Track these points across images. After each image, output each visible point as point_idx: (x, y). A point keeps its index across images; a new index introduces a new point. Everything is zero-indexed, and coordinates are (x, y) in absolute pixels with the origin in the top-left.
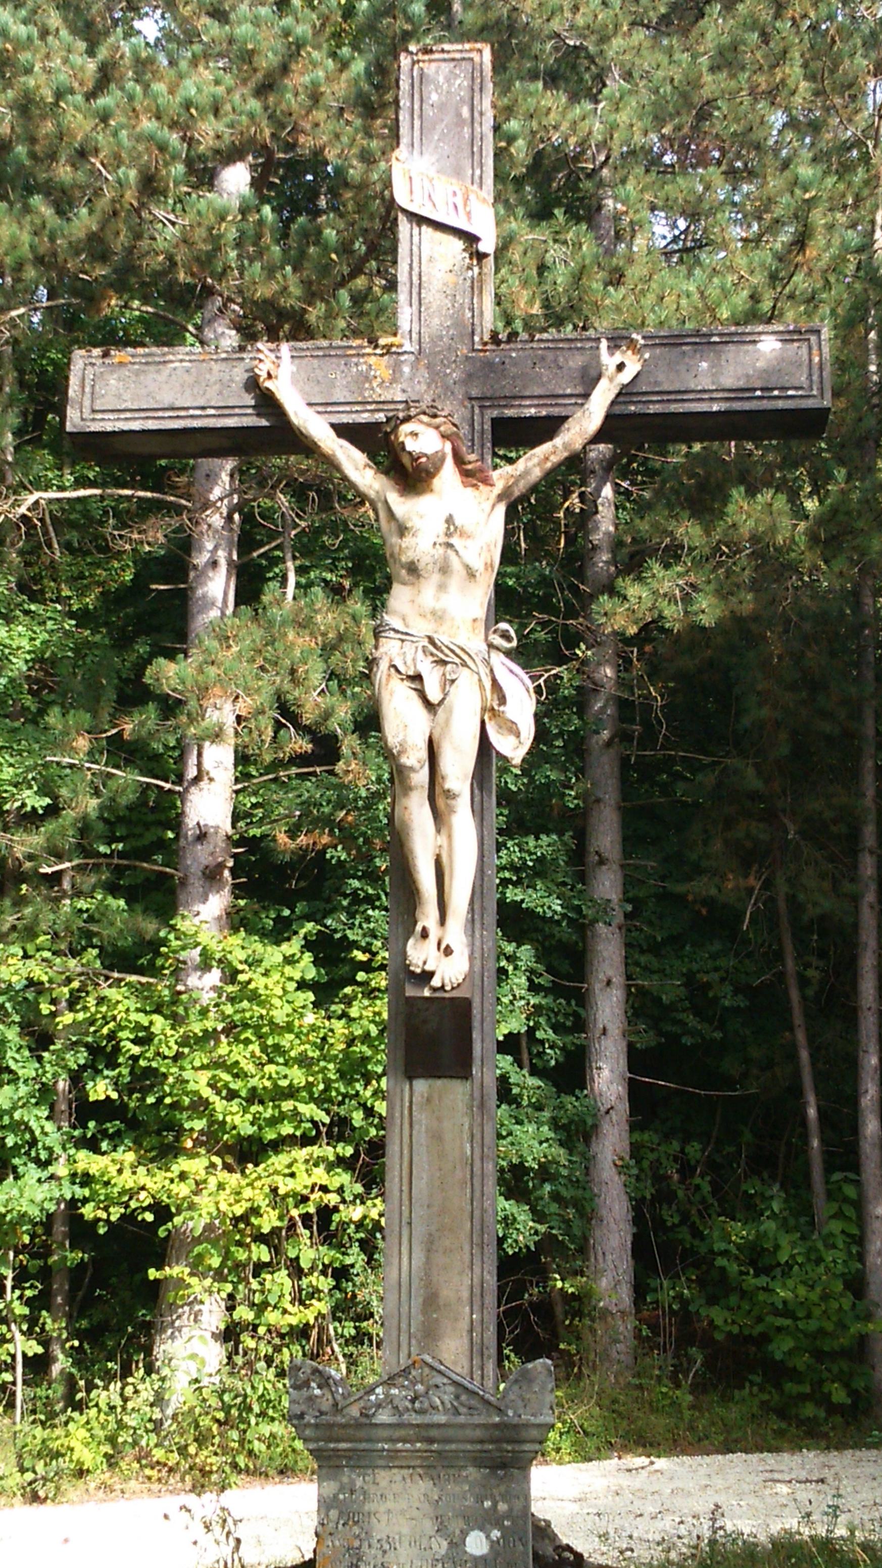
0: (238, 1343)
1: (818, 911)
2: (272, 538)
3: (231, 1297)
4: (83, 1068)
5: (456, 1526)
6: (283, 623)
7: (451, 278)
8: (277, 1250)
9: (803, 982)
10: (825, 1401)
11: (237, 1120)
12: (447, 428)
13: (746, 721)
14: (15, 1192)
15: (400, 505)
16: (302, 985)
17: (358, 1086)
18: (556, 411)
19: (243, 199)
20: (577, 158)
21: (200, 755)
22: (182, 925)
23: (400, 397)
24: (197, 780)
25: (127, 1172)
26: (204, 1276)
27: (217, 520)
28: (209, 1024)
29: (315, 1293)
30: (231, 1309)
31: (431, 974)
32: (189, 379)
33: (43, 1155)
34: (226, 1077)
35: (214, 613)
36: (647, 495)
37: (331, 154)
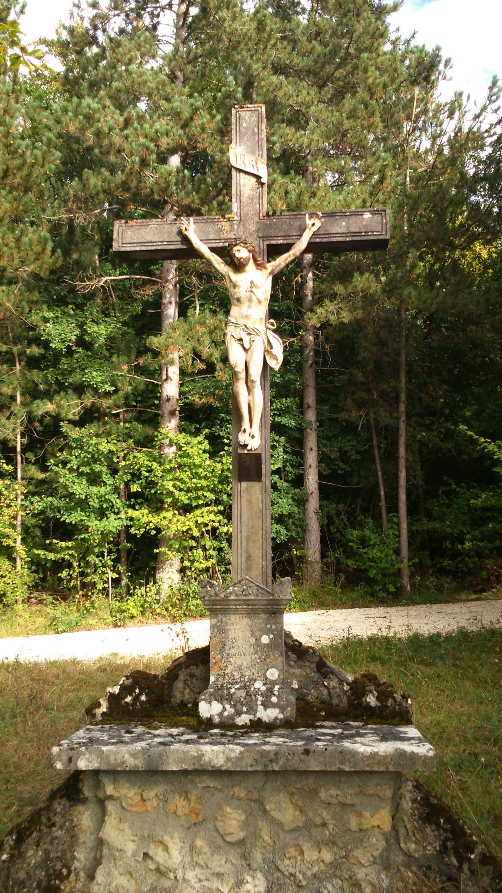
0: (185, 573)
1: (385, 423)
2: (190, 293)
3: (182, 558)
4: (129, 481)
5: (258, 634)
6: (195, 323)
7: (251, 192)
8: (198, 542)
9: (379, 448)
10: (387, 591)
11: (183, 498)
12: (251, 248)
13: (359, 358)
14: (107, 523)
15: (235, 277)
16: (204, 451)
17: (225, 486)
18: (290, 241)
19: (177, 167)
20: (300, 151)
21: (167, 371)
22: (163, 431)
23: (233, 237)
24: (166, 380)
25: (145, 517)
26: (173, 551)
27: (171, 287)
28: (172, 465)
29: (211, 557)
30: (182, 562)
31: (247, 445)
32: (156, 231)
33: (116, 510)
34: (179, 483)
35: (171, 320)
36: (325, 276)
37: (209, 151)
